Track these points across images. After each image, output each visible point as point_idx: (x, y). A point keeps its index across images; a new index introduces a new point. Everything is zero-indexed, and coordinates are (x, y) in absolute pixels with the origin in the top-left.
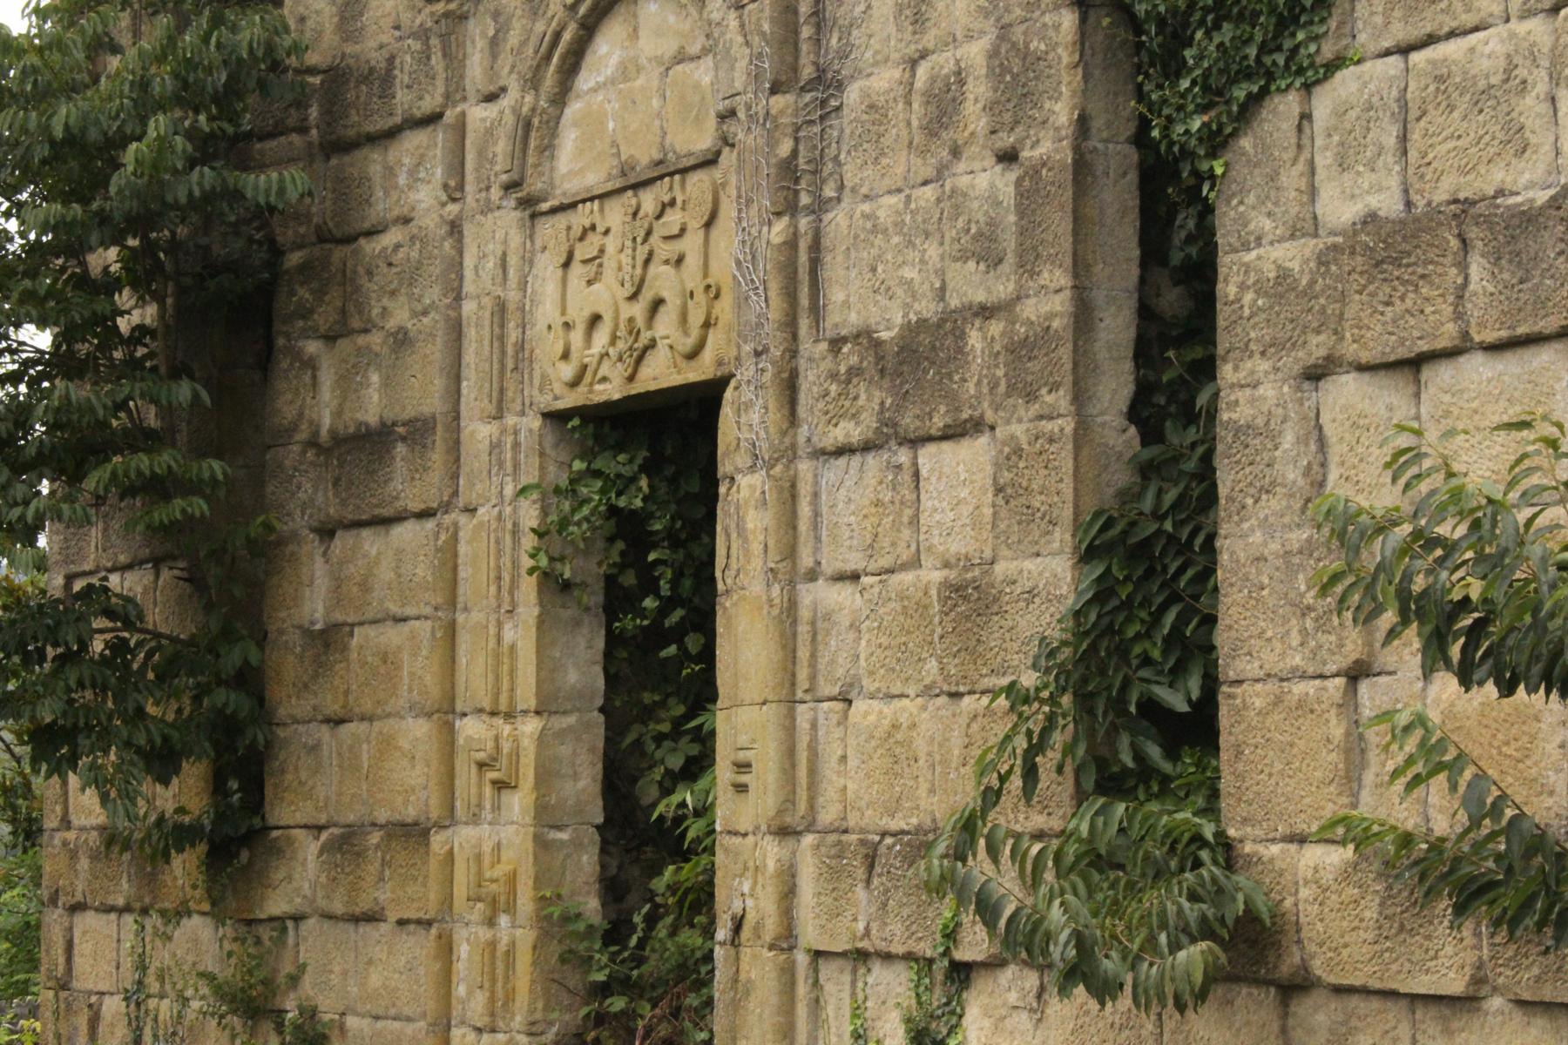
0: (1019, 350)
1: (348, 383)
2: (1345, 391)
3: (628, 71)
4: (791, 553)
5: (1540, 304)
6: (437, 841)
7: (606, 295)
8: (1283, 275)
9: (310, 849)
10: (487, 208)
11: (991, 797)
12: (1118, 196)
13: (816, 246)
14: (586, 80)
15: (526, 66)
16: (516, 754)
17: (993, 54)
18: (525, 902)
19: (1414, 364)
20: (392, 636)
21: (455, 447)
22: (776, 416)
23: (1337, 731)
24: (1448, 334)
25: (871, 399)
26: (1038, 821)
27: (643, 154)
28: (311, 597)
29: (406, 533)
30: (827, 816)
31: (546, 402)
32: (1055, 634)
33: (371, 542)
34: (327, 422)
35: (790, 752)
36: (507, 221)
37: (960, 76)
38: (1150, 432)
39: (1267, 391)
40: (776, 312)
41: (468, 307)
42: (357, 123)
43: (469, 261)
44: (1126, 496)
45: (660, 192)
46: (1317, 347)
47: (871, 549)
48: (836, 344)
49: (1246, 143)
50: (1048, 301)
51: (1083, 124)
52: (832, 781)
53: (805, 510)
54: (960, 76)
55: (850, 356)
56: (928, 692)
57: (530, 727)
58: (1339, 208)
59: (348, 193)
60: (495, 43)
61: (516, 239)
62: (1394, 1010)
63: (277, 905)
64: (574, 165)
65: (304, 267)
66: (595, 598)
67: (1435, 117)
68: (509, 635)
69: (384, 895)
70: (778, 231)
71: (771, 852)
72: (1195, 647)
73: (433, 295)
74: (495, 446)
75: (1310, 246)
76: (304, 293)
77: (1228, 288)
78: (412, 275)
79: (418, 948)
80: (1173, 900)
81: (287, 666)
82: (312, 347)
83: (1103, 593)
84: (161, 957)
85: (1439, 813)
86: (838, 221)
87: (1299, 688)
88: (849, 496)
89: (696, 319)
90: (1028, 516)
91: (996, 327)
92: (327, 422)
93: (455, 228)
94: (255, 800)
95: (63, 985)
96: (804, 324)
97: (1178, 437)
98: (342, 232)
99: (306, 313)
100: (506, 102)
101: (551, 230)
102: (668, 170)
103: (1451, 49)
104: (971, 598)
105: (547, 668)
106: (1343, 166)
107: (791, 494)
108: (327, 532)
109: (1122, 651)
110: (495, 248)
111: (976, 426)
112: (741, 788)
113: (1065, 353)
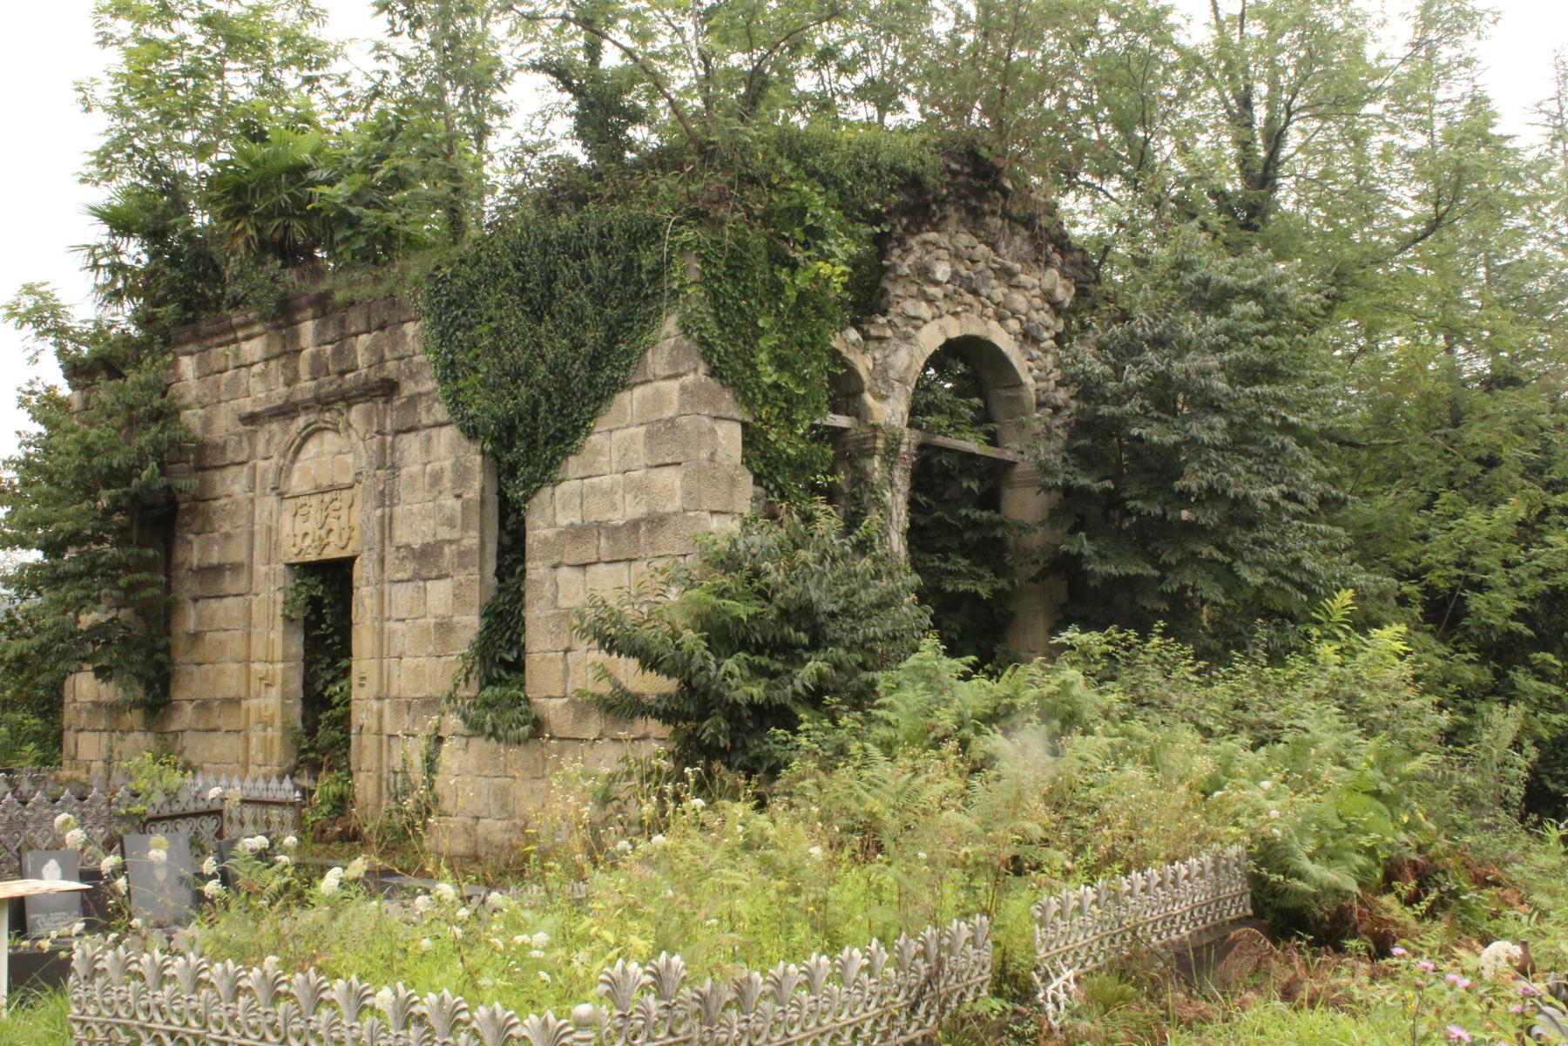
0: (462, 555)
1: (205, 549)
2: (564, 572)
3: (319, 455)
4: (382, 612)
5: (620, 552)
6: (244, 704)
7: (310, 526)
8: (546, 538)
9: (189, 709)
10: (265, 495)
11: (456, 686)
12: (493, 510)
13: (391, 518)
14: (302, 456)
15: (282, 448)
16: (274, 676)
17: (454, 465)
18: (278, 723)
19: (584, 566)
20: (223, 636)
21: (251, 574)
22: (377, 569)
23: (561, 666)
25: (410, 568)
26: (467, 693)
27: (325, 482)
28: (190, 620)
29: (228, 601)
30: (394, 693)
31: (286, 560)
32: (474, 639)
33: (214, 604)
34: (195, 562)
35: (381, 674)
36: (272, 500)
37: (442, 470)
38: (501, 580)
39: (541, 571)
40: (377, 537)
41: (257, 527)
42: (209, 461)
43: (257, 512)
44: (495, 598)
46: (556, 559)
47: (410, 612)
48: (398, 548)
49: (535, 500)
50: (472, 540)
51: (483, 489)
53: (386, 598)
54: (442, 470)
55: (403, 552)
56: (429, 655)
57: (280, 666)
58: (563, 520)
59: (204, 484)
60: (268, 441)
61: (275, 506)
63: (175, 727)
64: (297, 482)
65: (189, 510)
66: (301, 624)
68: (272, 635)
69: (220, 722)
70: (379, 512)
71: (375, 705)
72: (517, 643)
73: (242, 521)
74: (267, 574)
75: (555, 531)
76: (187, 518)
77: (529, 540)
78: (232, 515)
79: (236, 742)
80: (516, 713)
81: (180, 645)
82: (191, 536)
83: (488, 626)
84: (118, 747)
85: (604, 688)
86: (398, 510)
87: (550, 655)
88: (402, 597)
89: (345, 537)
90: (464, 604)
91: (454, 547)
92: (195, 562)
93: (252, 501)
94: (166, 691)
95: (74, 758)
96: (387, 542)
97: (510, 581)
98: (202, 498)
99: (189, 525)
100: (273, 461)
101: (287, 503)
102: (332, 488)
103: (596, 480)
104: (445, 628)
105: (286, 647)
106: (564, 508)
107: (382, 594)
108: (195, 600)
109: (493, 644)
110: (267, 508)
111: (447, 576)
112: (361, 685)
113: (477, 556)
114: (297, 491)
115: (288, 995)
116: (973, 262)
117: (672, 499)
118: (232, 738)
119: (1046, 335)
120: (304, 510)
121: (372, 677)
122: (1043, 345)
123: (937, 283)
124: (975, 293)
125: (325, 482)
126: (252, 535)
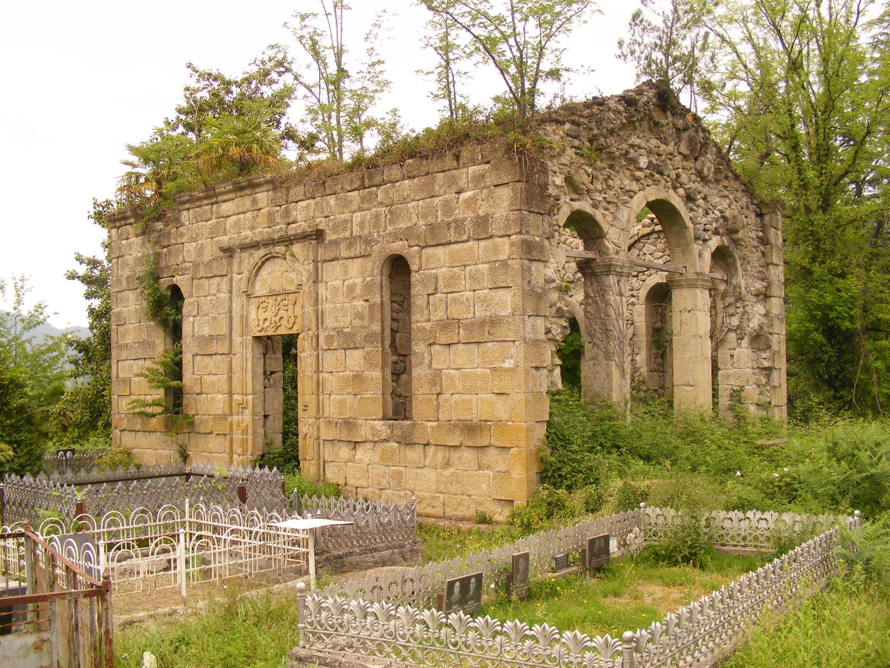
6: (229, 419)
7: (267, 315)
19: (449, 345)
23: (435, 403)
24: (456, 341)
30: (326, 415)
45: (283, 297)
46: (431, 341)
50: (376, 327)
52: (327, 409)
62: (446, 449)
64: (260, 289)
67: (453, 305)
89: (292, 321)
96: (320, 326)
100: (244, 275)
101: (252, 300)
114: (259, 294)
115: (447, 625)
116: (659, 155)
117: (505, 308)
118: (221, 438)
119: (699, 196)
120: (265, 305)
121: (312, 406)
122: (697, 202)
123: (640, 169)
124: (661, 173)
125: (277, 288)
126: (231, 318)
